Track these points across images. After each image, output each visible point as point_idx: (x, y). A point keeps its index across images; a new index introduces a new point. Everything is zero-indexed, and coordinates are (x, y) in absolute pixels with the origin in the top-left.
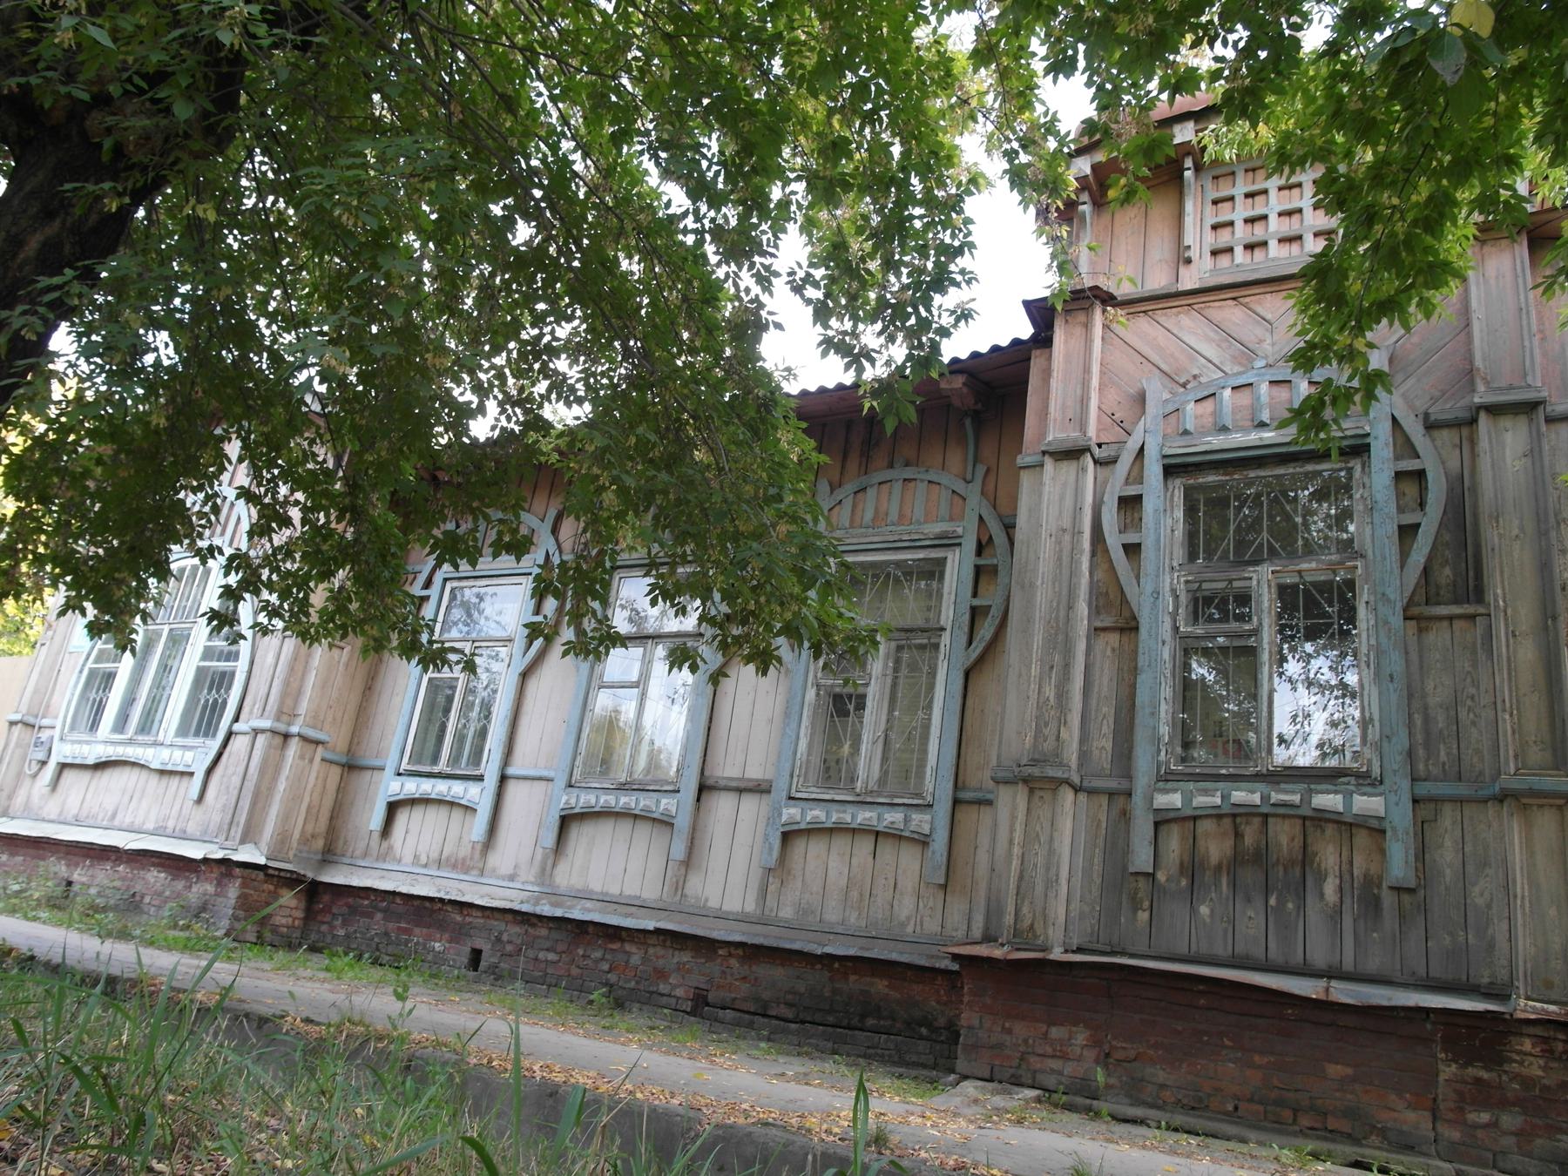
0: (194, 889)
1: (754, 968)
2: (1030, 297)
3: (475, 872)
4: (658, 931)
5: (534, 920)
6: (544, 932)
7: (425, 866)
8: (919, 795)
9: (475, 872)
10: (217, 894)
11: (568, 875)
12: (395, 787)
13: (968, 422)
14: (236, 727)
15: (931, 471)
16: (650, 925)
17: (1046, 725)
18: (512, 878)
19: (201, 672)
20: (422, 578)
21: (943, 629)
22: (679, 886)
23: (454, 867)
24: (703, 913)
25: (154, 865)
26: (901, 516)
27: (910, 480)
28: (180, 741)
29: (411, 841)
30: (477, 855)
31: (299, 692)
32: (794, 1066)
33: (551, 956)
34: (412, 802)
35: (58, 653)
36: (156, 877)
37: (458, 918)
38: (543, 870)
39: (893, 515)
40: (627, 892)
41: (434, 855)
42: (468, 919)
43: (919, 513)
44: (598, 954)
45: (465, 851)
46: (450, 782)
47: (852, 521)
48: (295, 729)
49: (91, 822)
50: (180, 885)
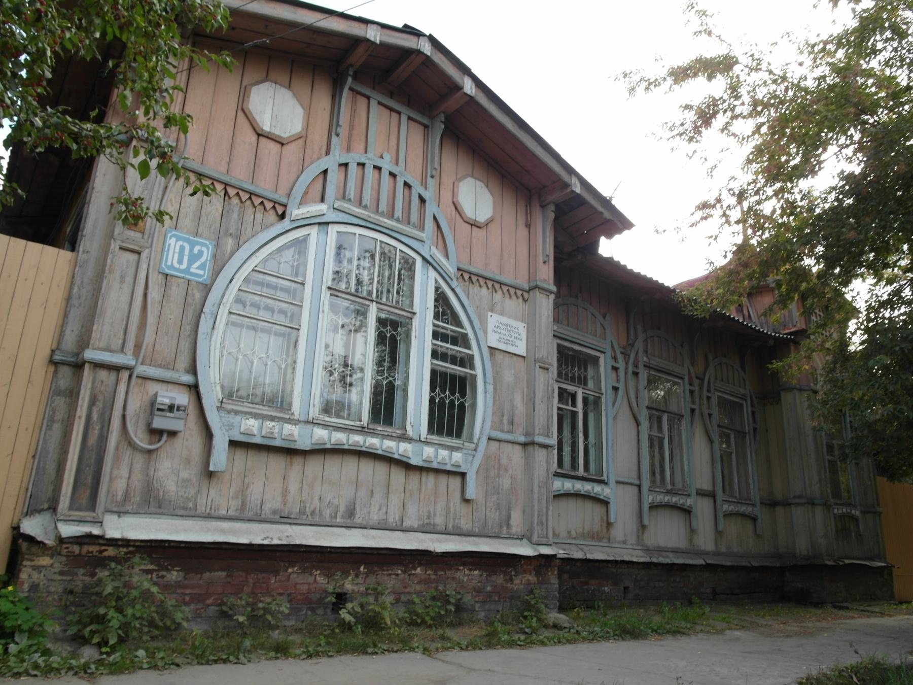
0: (517, 581)
2: (626, 233)
3: (605, 540)
7: (575, 538)
8: (750, 500)
9: (605, 540)
10: (540, 583)
16: (702, 562)
18: (625, 542)
19: (451, 363)
21: (648, 407)
22: (691, 540)
23: (593, 538)
24: (660, 550)
25: (464, 564)
28: (435, 438)
30: (605, 530)
33: (661, 584)
36: (469, 576)
37: (614, 570)
38: (638, 537)
41: (580, 531)
42: (620, 570)
44: (678, 580)
46: (595, 484)
49: (317, 519)
50: (500, 580)
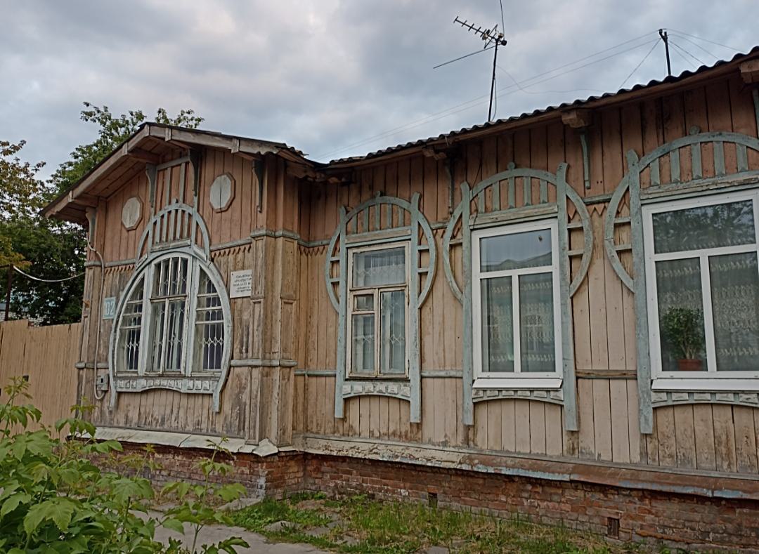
1: (654, 504)
4: (572, 481)
5: (472, 474)
6: (481, 481)
11: (485, 441)
12: (348, 389)
13: (583, 138)
14: (233, 363)
15: (724, 133)
17: (288, 274)
18: (445, 444)
20: (331, 248)
26: (704, 171)
27: (706, 143)
29: (365, 420)
31: (272, 338)
32: (154, 281)
34: (359, 397)
35: (96, 321)
39: (697, 171)
40: (535, 451)
43: (719, 167)
45: (405, 428)
47: (661, 180)
48: (276, 363)
